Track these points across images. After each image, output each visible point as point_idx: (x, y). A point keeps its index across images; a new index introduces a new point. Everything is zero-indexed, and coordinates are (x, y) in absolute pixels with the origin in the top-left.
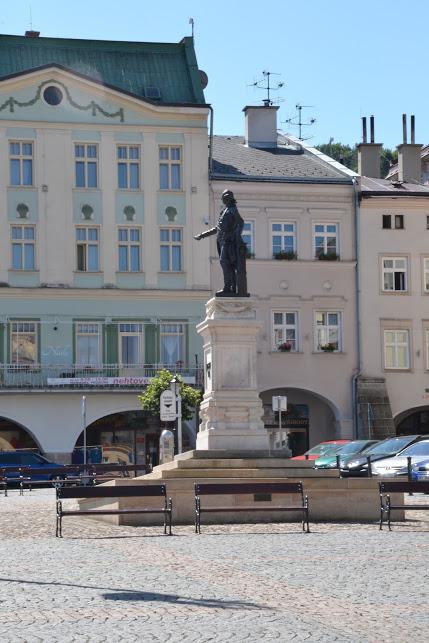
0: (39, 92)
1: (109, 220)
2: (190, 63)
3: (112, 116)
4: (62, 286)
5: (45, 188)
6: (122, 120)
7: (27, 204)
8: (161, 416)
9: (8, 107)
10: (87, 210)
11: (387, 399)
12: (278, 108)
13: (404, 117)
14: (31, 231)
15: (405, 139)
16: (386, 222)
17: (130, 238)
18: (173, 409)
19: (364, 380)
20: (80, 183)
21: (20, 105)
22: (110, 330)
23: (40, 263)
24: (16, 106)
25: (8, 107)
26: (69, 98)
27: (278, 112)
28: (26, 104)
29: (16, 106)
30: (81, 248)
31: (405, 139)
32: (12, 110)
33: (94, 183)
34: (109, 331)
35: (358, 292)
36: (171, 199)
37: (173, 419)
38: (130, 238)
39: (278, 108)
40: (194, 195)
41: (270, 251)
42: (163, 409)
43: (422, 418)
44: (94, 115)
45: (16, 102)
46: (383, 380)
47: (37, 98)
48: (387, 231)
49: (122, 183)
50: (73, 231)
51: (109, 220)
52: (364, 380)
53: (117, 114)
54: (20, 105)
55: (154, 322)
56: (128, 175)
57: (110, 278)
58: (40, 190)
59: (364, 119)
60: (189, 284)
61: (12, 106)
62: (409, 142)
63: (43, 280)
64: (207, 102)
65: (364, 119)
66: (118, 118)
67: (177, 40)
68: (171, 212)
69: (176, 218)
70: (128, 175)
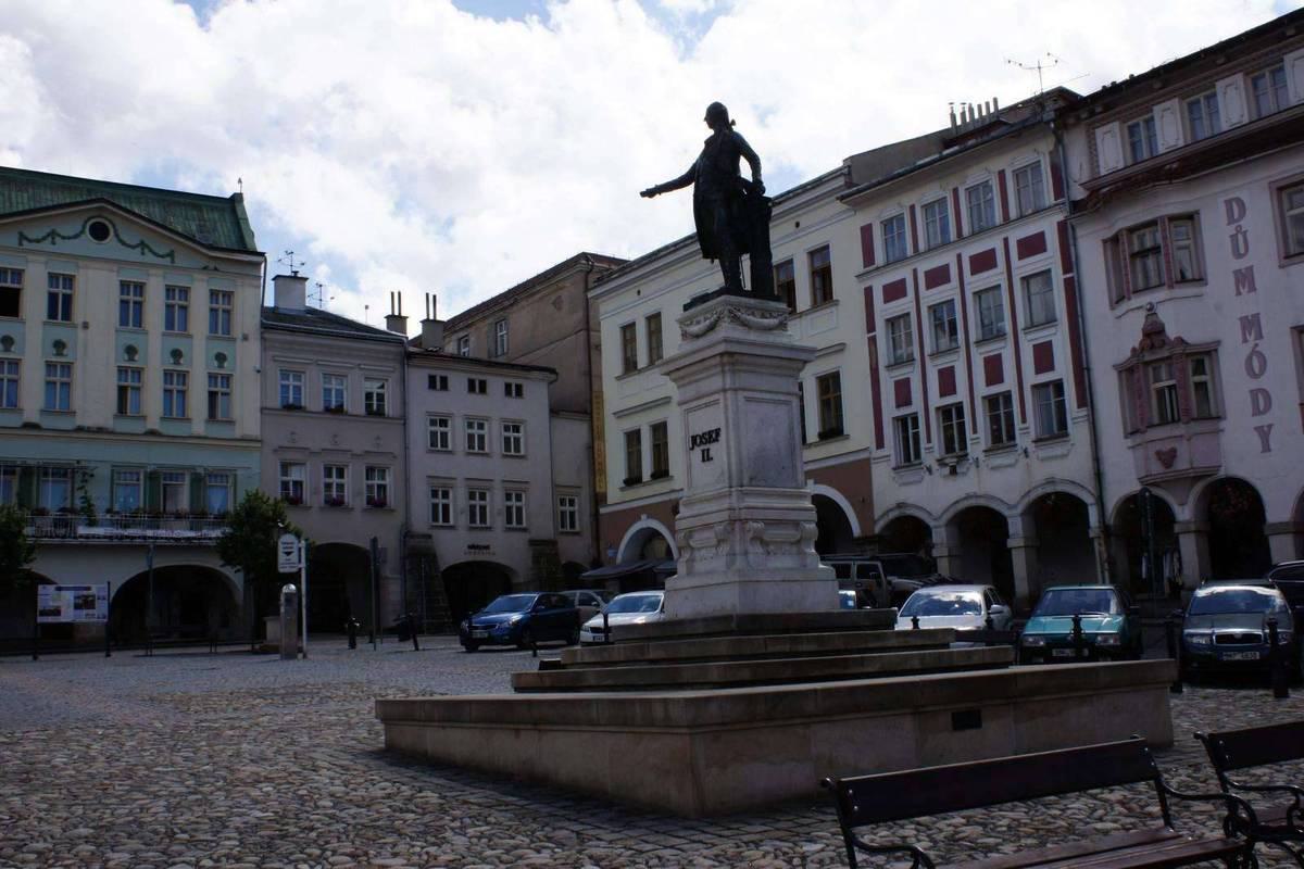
0: (84, 227)
1: (154, 361)
2: (240, 216)
3: (162, 257)
4: (100, 430)
5: (86, 326)
6: (173, 262)
7: (64, 340)
8: (280, 566)
9: (50, 239)
10: (131, 351)
11: (435, 556)
12: (306, 279)
13: (427, 295)
14: (67, 368)
15: (428, 315)
16: (432, 384)
17: (176, 379)
18: (294, 557)
19: (412, 537)
20: (124, 321)
21: (64, 238)
22: (153, 477)
23: (77, 402)
24: (57, 239)
25: (50, 239)
26: (117, 235)
27: (307, 283)
28: (69, 238)
29: (57, 239)
30: (122, 391)
31: (428, 315)
32: (54, 243)
33: (139, 322)
34: (151, 478)
35: (406, 448)
36: (221, 347)
37: (295, 570)
38: (176, 379)
39: (306, 279)
40: (246, 343)
41: (320, 407)
42: (282, 558)
43: (1097, 618)
44: (143, 254)
45: (59, 235)
46: (430, 537)
47: (82, 232)
48: (433, 392)
49: (170, 324)
50: (115, 371)
51: (154, 361)
52: (412, 537)
53: (168, 255)
54: (64, 238)
55: (201, 471)
56: (177, 316)
57: (154, 422)
58: (80, 327)
59: (392, 294)
60: (238, 434)
61: (53, 238)
62: (431, 317)
63: (79, 421)
64: (259, 250)
65: (392, 294)
66: (168, 259)
67: (228, 195)
68: (221, 358)
69: (226, 364)
70: (177, 316)
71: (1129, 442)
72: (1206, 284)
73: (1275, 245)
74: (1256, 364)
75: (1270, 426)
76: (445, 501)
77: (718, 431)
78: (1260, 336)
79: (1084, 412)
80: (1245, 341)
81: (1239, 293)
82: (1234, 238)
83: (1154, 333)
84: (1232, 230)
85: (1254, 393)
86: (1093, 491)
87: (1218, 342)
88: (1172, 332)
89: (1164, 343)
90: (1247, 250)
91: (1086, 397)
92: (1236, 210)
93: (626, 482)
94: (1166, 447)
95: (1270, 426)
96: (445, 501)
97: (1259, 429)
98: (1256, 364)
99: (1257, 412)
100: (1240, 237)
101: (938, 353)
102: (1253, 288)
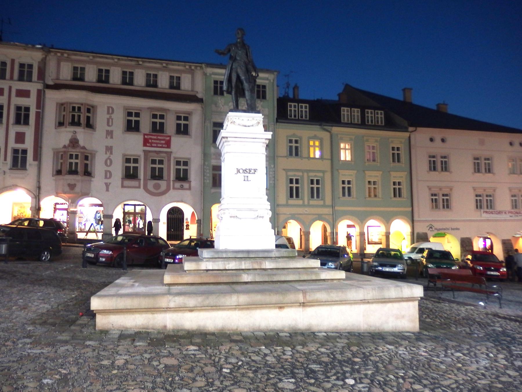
71: (54, 178)
72: (95, 131)
73: (300, 125)
74: (108, 162)
75: (110, 183)
76: (394, 152)
77: (255, 170)
78: (111, 153)
79: (36, 163)
80: (106, 153)
81: (107, 138)
82: (108, 120)
83: (74, 142)
84: (108, 116)
85: (106, 172)
86: (34, 193)
87: (451, 172)
88: (81, 143)
89: (78, 146)
90: (112, 124)
91: (37, 157)
92: (110, 110)
93: (349, 234)
94: (73, 182)
95: (110, 183)
96: (394, 152)
97: (106, 184)
98: (108, 162)
99: (106, 177)
100: (111, 120)
101: (351, 123)
102: (112, 137)
